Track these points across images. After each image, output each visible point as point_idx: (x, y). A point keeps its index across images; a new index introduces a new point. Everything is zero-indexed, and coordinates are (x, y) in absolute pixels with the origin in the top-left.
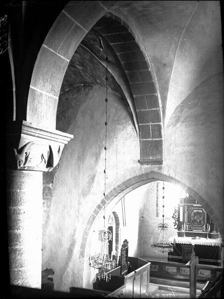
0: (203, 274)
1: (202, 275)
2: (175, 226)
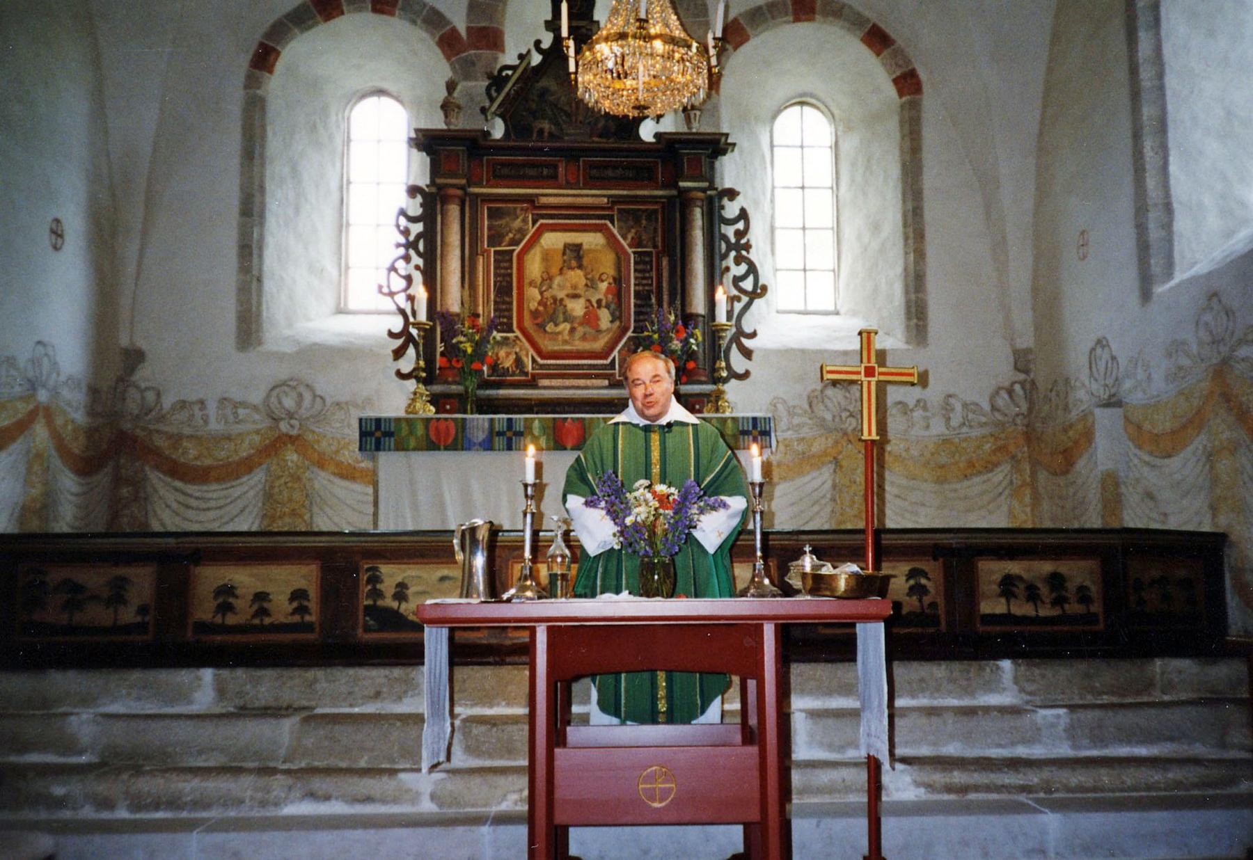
2: (398, 353)
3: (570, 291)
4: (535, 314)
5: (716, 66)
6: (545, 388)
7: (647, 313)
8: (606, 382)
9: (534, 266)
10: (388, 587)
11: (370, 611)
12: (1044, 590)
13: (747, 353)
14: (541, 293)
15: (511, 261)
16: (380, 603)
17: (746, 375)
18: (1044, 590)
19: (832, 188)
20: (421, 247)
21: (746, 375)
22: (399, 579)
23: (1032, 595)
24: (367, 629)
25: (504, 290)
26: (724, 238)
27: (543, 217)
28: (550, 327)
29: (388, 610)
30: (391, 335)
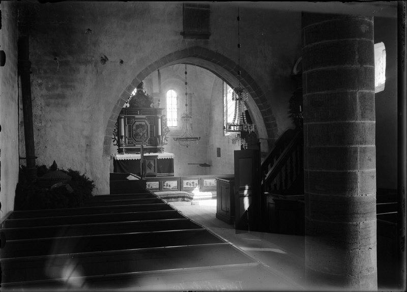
0: (170, 186)
1: (168, 187)
2: (114, 141)
4: (135, 135)
9: (134, 128)
12: (192, 184)
13: (167, 141)
18: (192, 184)
23: (190, 185)
25: (129, 131)
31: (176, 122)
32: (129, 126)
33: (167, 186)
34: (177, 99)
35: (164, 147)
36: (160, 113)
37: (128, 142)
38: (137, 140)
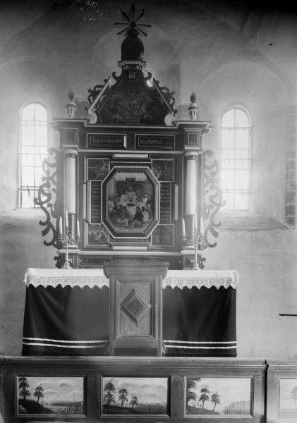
0: (215, 399)
2: (45, 233)
3: (129, 202)
5: (71, 155)
6: (116, 250)
7: (167, 214)
8: (146, 248)
10: (32, 389)
11: (23, 402)
13: (216, 235)
14: (115, 204)
15: (100, 187)
16: (27, 398)
17: (215, 245)
19: (249, 149)
20: (55, 179)
21: (215, 245)
22: (38, 385)
24: (21, 412)
26: (206, 176)
27: (116, 164)
28: (119, 221)
29: (32, 402)
30: (41, 223)
31: (246, 197)
32: (96, 186)
33: (203, 398)
34: (251, 134)
35: (205, 253)
36: (194, 140)
37: (91, 239)
38: (117, 230)
